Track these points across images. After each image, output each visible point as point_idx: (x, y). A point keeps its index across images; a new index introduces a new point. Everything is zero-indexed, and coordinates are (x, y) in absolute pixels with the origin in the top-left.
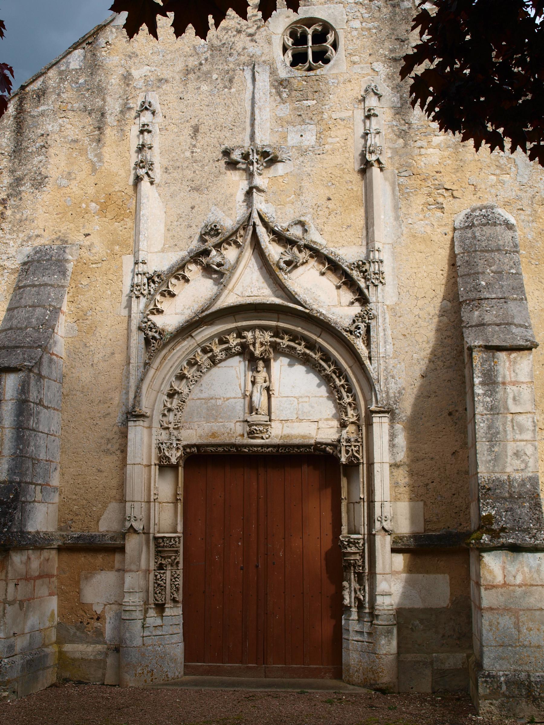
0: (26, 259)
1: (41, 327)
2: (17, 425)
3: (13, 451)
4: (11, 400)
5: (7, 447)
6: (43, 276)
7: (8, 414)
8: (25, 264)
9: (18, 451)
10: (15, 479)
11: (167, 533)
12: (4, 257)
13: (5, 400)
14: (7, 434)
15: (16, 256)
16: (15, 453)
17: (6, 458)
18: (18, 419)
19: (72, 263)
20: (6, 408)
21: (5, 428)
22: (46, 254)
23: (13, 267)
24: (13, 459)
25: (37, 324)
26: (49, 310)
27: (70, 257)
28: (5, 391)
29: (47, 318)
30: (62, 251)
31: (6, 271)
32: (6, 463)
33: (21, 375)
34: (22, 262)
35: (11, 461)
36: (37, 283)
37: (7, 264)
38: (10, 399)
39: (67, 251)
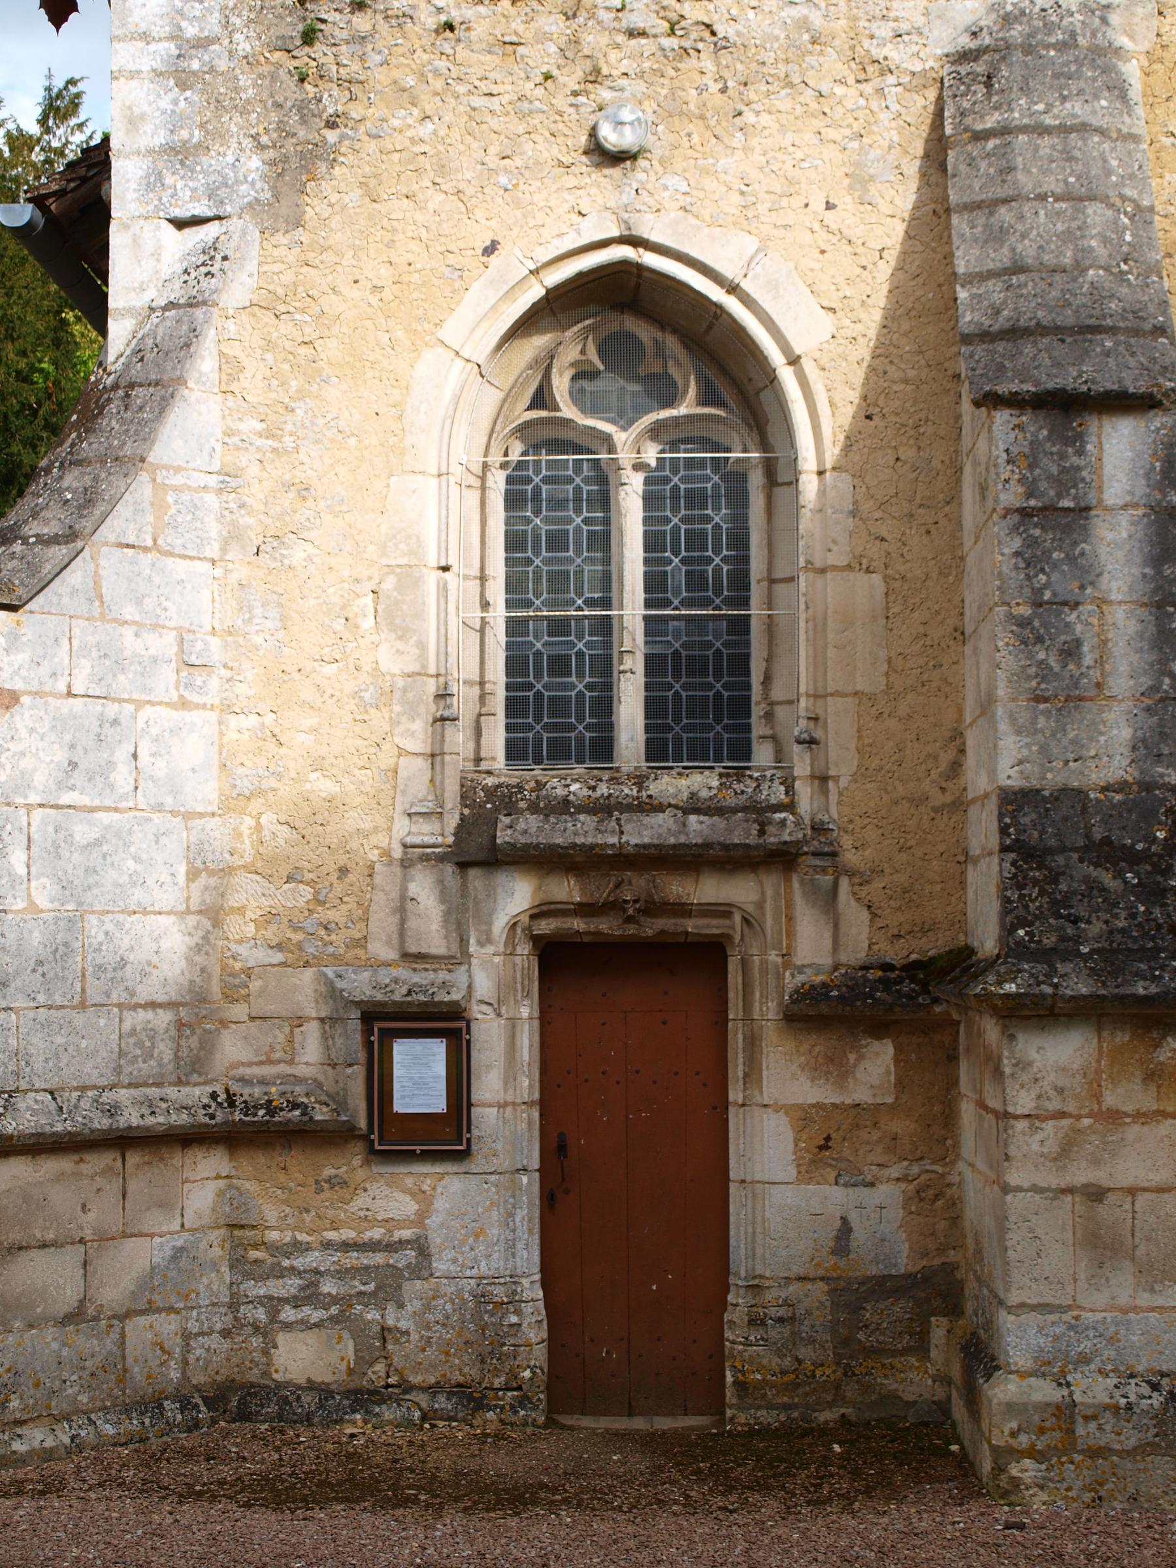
0: (966, 42)
1: (1124, 267)
2: (1154, 592)
3: (1146, 682)
4: (1125, 507)
5: (1123, 668)
6: (1064, 99)
7: (1120, 554)
8: (964, 56)
9: (1167, 681)
10: (1162, 776)
11: (250, 1064)
12: (884, 30)
13: (1106, 509)
14: (1121, 624)
15: (926, 30)
16: (1155, 688)
17: (1124, 706)
18: (1159, 572)
19: (1134, 61)
20: (1110, 536)
21: (1111, 603)
22: (1049, 28)
23: (918, 67)
24: (1148, 709)
25: (1110, 256)
26: (1126, 213)
27: (1124, 41)
28: (1100, 477)
29: (1128, 238)
30: (1097, 21)
31: (891, 79)
32: (1123, 723)
33: (1158, 420)
34: (950, 49)
35: (1142, 715)
36: (1048, 121)
37: (894, 53)
38: (1120, 502)
39: (1115, 18)
